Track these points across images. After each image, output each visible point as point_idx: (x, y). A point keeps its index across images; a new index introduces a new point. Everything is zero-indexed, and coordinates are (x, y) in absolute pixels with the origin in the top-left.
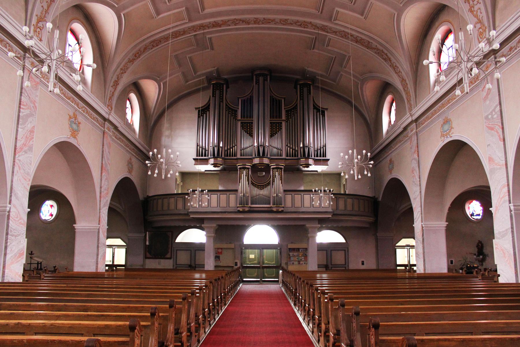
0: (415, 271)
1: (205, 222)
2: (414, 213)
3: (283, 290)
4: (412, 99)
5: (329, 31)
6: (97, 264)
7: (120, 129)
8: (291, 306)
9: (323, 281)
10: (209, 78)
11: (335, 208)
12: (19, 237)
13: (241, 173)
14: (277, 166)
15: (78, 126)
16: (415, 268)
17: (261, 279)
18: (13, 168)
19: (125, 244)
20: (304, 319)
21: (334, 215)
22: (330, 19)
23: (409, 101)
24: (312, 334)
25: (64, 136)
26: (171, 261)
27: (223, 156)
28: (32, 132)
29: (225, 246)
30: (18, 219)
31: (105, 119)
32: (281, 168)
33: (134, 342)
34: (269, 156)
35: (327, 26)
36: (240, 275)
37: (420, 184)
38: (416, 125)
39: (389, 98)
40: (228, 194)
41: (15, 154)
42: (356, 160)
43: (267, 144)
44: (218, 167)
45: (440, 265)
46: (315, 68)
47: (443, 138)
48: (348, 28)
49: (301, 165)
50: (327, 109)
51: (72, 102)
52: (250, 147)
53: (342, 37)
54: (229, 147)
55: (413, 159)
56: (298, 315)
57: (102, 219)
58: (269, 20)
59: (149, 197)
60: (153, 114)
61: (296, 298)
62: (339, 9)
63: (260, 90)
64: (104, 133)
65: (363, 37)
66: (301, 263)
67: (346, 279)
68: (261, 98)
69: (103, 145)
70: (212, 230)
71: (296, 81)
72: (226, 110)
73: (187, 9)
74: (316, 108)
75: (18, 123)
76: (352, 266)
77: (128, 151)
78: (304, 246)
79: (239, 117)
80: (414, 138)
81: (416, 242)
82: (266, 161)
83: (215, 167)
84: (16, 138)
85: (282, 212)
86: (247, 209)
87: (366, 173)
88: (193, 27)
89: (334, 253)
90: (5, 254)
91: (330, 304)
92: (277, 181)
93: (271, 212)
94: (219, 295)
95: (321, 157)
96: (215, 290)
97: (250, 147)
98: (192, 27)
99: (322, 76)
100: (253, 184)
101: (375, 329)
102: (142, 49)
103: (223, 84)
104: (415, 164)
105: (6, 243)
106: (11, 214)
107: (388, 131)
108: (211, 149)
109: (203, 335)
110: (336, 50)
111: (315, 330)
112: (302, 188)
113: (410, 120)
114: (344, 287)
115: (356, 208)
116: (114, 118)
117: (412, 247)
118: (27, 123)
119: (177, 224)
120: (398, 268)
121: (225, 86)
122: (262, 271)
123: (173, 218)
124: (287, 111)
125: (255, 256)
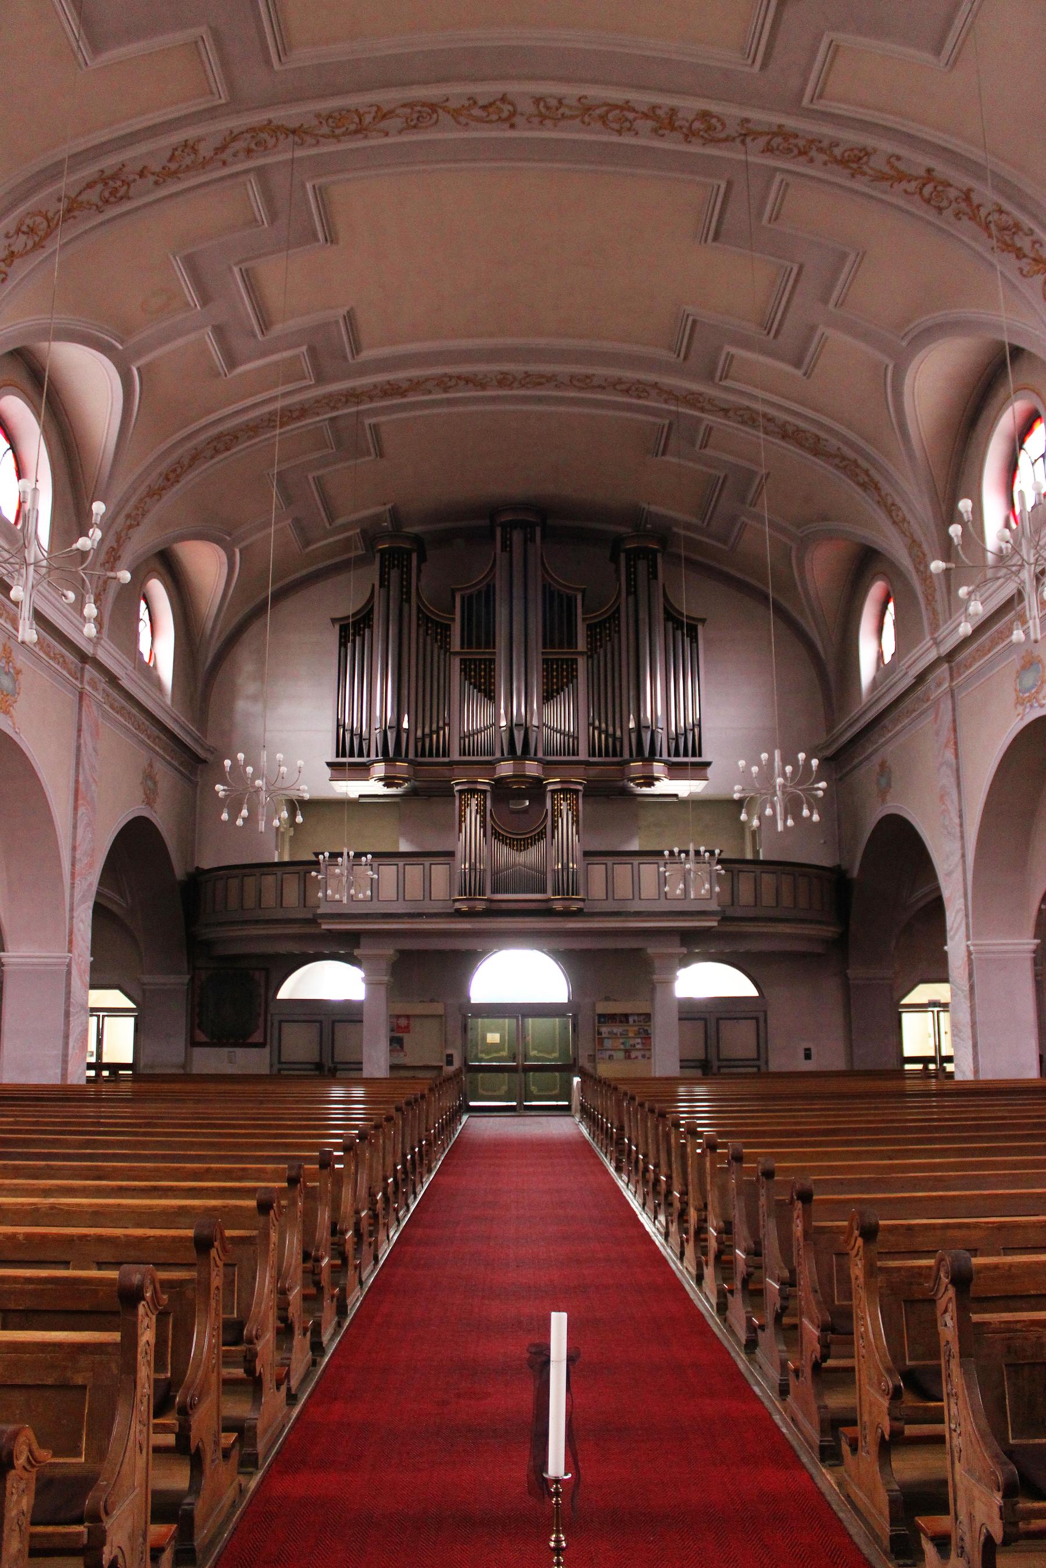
0: (951, 1075)
1: (363, 941)
2: (948, 914)
3: (585, 1132)
4: (938, 596)
5: (708, 407)
6: (65, 1062)
7: (125, 682)
8: (606, 1172)
9: (697, 1106)
10: (370, 535)
11: (727, 899)
13: (464, 806)
14: (565, 786)
15: (15, 681)
16: (950, 1067)
17: (520, 1103)
19: (131, 1005)
20: (644, 1205)
21: (725, 919)
22: (709, 376)
23: (930, 600)
24: (666, 1239)
26: (266, 1051)
27: (411, 756)
29: (419, 1009)
32: (576, 792)
33: (267, 1236)
34: (540, 755)
35: (701, 394)
36: (461, 1091)
37: (962, 832)
38: (951, 669)
39: (876, 590)
42: (779, 780)
43: (535, 722)
44: (398, 785)
45: (1018, 1059)
46: (669, 508)
47: (1020, 709)
48: (755, 398)
49: (632, 780)
50: (703, 621)
52: (486, 728)
54: (427, 731)
55: (941, 765)
56: (629, 1195)
59: (199, 871)
60: (211, 635)
61: (621, 1152)
62: (733, 350)
63: (515, 573)
65: (803, 425)
66: (633, 1054)
67: (758, 1099)
68: (517, 591)
69: (79, 730)
70: (384, 965)
71: (616, 543)
72: (418, 625)
73: (313, 351)
74: (672, 617)
76: (777, 1063)
77: (143, 742)
78: (642, 1007)
79: (456, 644)
80: (946, 706)
81: (953, 995)
82: (532, 768)
85: (579, 913)
86: (480, 906)
87: (806, 812)
88: (330, 396)
89: (726, 1027)
91: (708, 1159)
92: (566, 825)
93: (548, 913)
94: (416, 1143)
95: (688, 758)
96: (408, 1131)
97: (486, 728)
98: (324, 397)
99: (688, 526)
100: (496, 835)
101: (803, 1203)
102: (186, 461)
103: (409, 553)
104: (947, 780)
107: (875, 684)
108: (377, 735)
109: (385, 1246)
110: (726, 457)
111: (673, 1228)
112: (635, 846)
113: (933, 655)
114: (758, 1118)
115: (787, 901)
116: (108, 655)
117: (945, 1006)
119: (283, 948)
120: (908, 1067)
121: (414, 556)
122: (525, 1079)
124: (590, 627)
125: (502, 1038)
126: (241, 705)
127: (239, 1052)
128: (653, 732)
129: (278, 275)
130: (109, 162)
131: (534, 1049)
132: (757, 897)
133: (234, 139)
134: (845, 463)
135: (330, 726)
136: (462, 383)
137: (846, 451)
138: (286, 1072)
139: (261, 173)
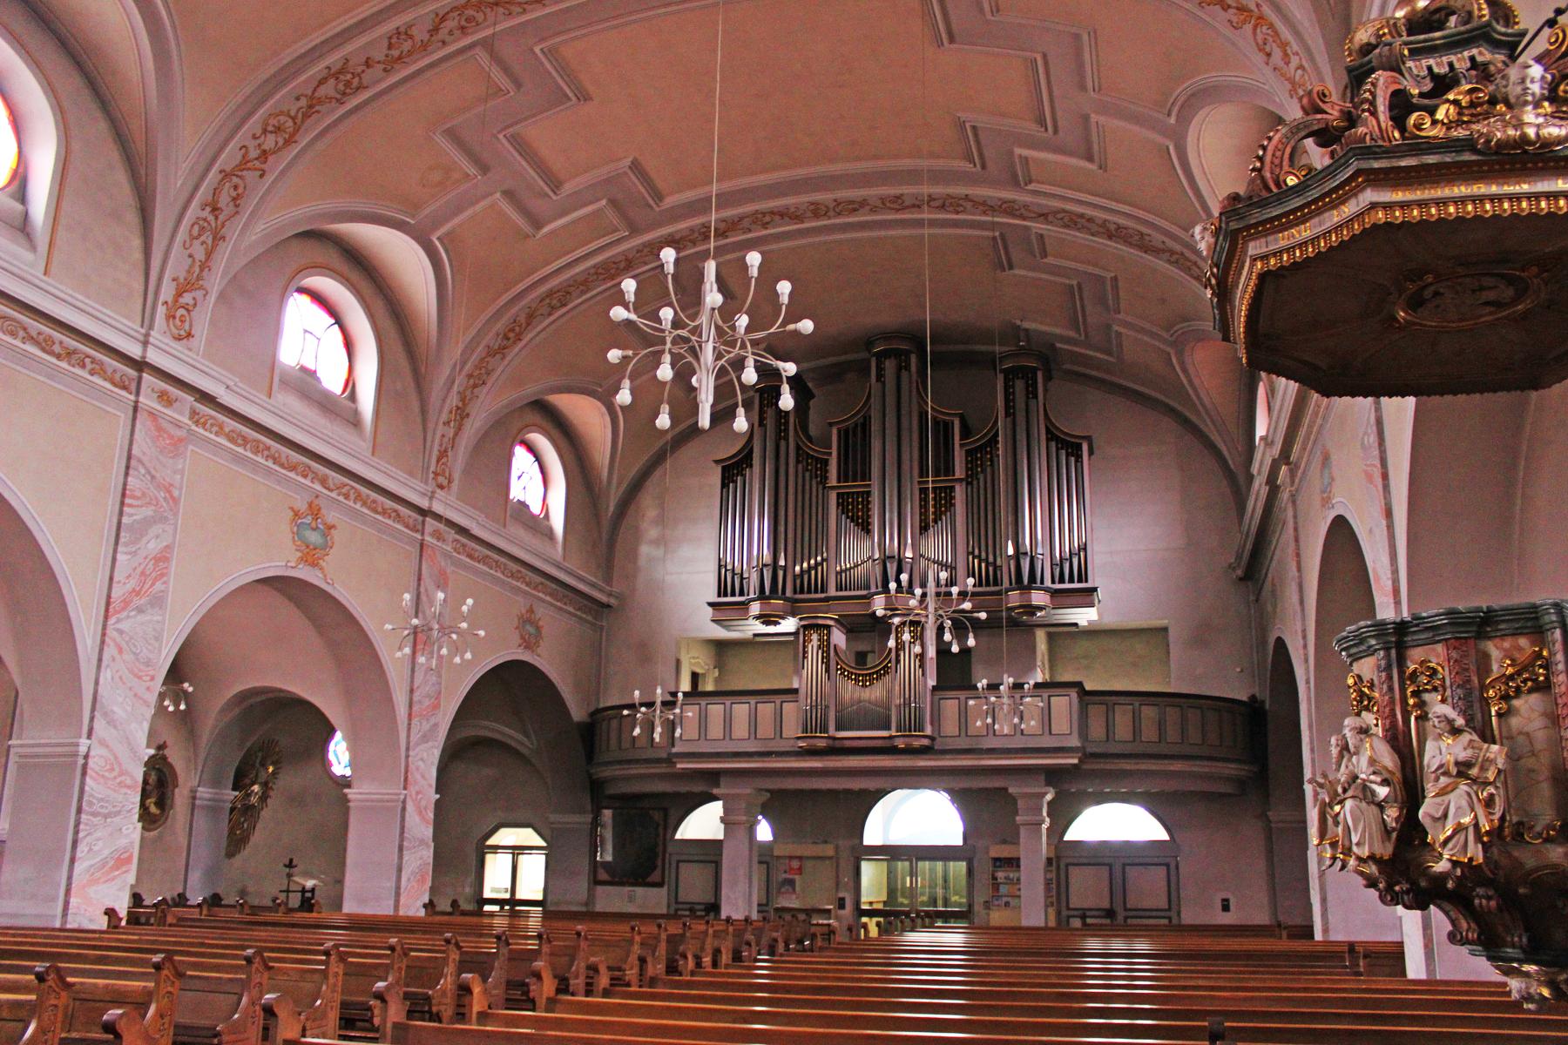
1: (723, 781)
12: (117, 819)
15: (325, 535)
18: (101, 650)
22: (1015, 182)
25: (282, 561)
26: (664, 890)
27: (789, 593)
28: (162, 558)
30: (115, 773)
31: (424, 512)
40: (728, 703)
41: (106, 617)
43: (909, 554)
51: (305, 476)
53: (1066, 226)
57: (415, 776)
58: (852, 202)
62: (1025, 152)
64: (422, 546)
65: (1122, 221)
72: (798, 462)
73: (613, 202)
75: (117, 543)
76: (1189, 917)
79: (833, 481)
83: (767, 623)
84: (111, 579)
86: (822, 744)
90: (73, 860)
93: (892, 751)
99: (1068, 340)
102: (522, 319)
105: (76, 832)
106: (91, 762)
115: (1172, 734)
118: (145, 540)
123: (1108, 767)
126: (645, 550)
127: (639, 891)
128: (1032, 558)
129: (544, 134)
130: (333, 59)
131: (903, 896)
132: (1136, 731)
133: (443, 19)
134: (1175, 257)
135: (713, 566)
136: (777, 218)
137: (1170, 243)
138: (1135, 921)
139: (487, 44)
